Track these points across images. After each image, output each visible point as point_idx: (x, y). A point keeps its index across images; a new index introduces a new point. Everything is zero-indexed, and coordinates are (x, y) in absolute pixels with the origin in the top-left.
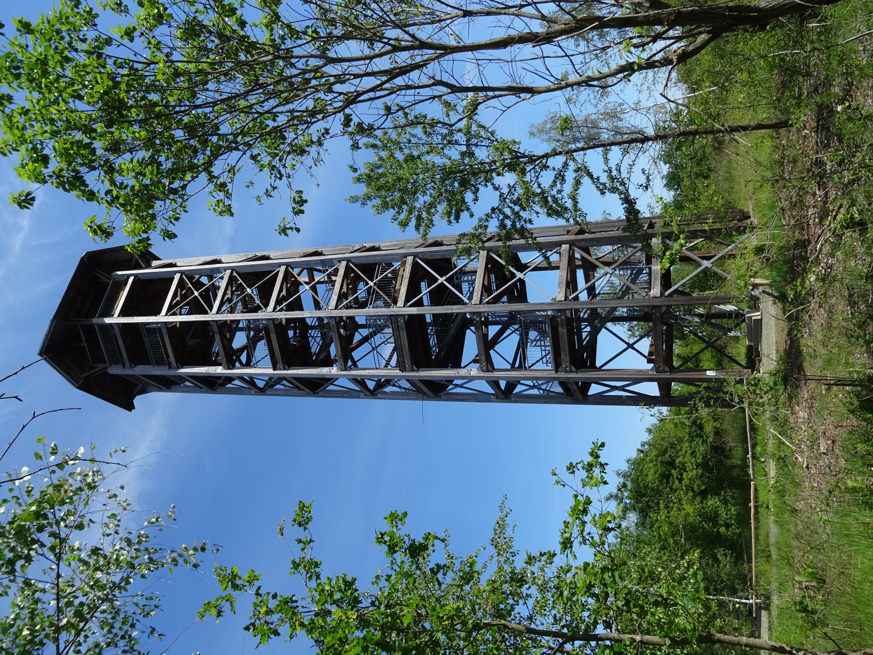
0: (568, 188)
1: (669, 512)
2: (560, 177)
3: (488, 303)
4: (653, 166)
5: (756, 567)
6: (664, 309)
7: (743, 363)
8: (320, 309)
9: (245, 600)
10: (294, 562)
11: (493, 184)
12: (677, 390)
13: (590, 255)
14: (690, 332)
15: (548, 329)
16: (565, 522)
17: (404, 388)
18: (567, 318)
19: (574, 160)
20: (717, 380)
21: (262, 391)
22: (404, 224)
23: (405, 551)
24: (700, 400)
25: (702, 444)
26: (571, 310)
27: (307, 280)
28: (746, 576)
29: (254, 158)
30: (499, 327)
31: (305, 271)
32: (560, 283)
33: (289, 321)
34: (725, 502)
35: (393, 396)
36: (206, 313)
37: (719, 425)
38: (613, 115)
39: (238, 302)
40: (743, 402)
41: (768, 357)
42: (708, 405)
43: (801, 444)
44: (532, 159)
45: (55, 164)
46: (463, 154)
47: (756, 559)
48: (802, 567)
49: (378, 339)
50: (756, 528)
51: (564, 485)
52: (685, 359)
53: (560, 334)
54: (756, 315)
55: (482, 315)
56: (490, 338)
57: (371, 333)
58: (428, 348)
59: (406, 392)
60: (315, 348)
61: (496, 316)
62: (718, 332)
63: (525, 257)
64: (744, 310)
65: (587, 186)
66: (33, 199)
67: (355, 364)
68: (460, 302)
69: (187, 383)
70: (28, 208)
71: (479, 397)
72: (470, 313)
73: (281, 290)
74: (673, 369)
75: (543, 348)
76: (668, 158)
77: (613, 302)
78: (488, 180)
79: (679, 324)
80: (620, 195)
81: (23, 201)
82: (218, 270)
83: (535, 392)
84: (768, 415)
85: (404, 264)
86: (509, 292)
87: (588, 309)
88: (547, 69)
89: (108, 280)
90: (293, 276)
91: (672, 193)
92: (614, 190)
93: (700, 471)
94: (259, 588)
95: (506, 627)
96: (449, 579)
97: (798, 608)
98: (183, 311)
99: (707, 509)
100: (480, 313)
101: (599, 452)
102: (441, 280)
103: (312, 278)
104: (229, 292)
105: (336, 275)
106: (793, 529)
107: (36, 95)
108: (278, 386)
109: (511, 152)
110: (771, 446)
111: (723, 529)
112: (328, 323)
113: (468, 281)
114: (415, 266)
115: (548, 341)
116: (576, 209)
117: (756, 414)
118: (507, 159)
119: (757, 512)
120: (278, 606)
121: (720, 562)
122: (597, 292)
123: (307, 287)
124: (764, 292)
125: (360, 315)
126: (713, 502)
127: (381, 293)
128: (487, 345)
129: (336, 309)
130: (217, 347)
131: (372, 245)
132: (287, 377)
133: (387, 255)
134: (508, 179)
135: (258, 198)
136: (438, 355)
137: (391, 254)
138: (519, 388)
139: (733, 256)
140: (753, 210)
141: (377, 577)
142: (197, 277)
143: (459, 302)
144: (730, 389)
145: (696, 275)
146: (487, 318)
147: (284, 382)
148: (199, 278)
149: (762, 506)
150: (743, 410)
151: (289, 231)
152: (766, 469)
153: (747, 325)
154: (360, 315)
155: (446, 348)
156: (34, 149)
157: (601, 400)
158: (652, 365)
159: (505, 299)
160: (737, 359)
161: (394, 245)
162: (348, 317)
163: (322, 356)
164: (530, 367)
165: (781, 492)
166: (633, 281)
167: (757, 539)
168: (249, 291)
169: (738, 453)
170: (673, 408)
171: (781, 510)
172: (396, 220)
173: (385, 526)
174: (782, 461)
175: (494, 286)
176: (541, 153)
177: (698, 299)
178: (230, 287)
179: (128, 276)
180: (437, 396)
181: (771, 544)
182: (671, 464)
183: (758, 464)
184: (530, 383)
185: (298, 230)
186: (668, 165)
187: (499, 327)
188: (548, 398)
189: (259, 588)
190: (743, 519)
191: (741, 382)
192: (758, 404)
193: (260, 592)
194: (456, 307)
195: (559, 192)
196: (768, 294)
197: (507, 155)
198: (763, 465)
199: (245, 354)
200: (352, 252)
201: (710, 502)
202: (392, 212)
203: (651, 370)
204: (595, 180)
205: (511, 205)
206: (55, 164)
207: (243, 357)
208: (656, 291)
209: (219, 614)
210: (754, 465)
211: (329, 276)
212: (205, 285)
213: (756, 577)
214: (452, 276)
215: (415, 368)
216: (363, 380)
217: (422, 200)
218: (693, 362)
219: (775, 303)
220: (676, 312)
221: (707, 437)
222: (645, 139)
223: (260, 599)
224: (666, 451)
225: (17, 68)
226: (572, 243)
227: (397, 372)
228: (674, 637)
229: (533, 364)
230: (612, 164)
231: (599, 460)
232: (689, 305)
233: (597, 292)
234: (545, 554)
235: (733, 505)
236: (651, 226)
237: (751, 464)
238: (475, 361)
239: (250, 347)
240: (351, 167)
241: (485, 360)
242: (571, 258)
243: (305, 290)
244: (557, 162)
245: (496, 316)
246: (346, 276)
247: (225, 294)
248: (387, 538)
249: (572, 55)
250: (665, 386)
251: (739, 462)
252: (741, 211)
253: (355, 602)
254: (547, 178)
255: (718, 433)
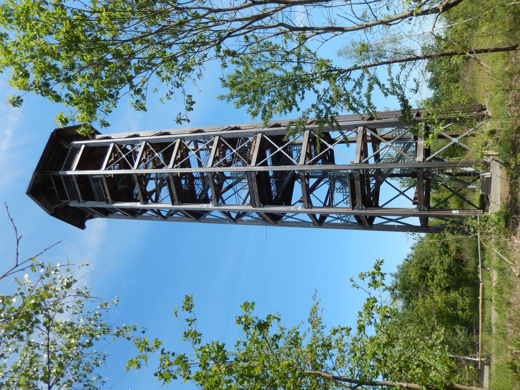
0: (364, 90)
1: (424, 300)
2: (359, 84)
3: (309, 164)
4: (422, 77)
5: (482, 337)
6: (425, 170)
7: (477, 205)
8: (202, 167)
9: (155, 358)
10: (185, 333)
11: (314, 89)
12: (432, 222)
13: (377, 133)
14: (443, 185)
15: (348, 181)
16: (359, 312)
17: (255, 218)
18: (360, 174)
19: (368, 72)
20: (460, 217)
21: (165, 218)
22: (255, 114)
23: (256, 327)
24: (447, 230)
25: (448, 257)
26: (363, 169)
27: (194, 148)
28: (474, 343)
29: (158, 73)
30: (316, 179)
31: (192, 142)
32: (356, 152)
33: (182, 174)
34: (462, 295)
35: (249, 223)
36: (129, 168)
37: (459, 245)
38: (394, 41)
39: (150, 162)
40: (476, 232)
41: (495, 203)
42: (452, 233)
43: (515, 261)
44: (341, 71)
45: (34, 77)
46: (296, 69)
47: (482, 332)
48: (513, 340)
49: (238, 186)
50: (483, 313)
51: (358, 288)
52: (438, 201)
53: (356, 185)
54: (487, 175)
55: (305, 172)
56: (310, 186)
57: (234, 182)
58: (270, 192)
59: (255, 220)
60: (198, 191)
61: (314, 173)
62: (461, 186)
63: (335, 135)
64: (479, 171)
65: (376, 90)
66: (22, 101)
67: (223, 201)
68: (291, 163)
69: (118, 213)
70: (18, 106)
71: (302, 224)
72: (297, 171)
73: (177, 155)
74: (429, 209)
75: (344, 194)
76: (430, 68)
77: (391, 164)
78: (310, 86)
79: (435, 180)
80: (398, 96)
81: (15, 102)
82: (138, 142)
83: (339, 221)
84: (493, 241)
85: (255, 138)
86: (323, 157)
87: (374, 169)
88: (353, 13)
89: (68, 147)
90: (185, 146)
91: (433, 91)
92: (393, 93)
93: (446, 275)
94: (163, 350)
95: (320, 375)
96: (281, 343)
97: (509, 366)
98: (116, 167)
99: (450, 299)
100: (304, 171)
101: (381, 267)
102: (279, 149)
103: (196, 147)
104: (144, 155)
105: (212, 145)
106: (508, 315)
107: (22, 33)
108: (175, 215)
109: (327, 67)
110: (495, 261)
111: (460, 313)
112: (207, 176)
113: (296, 150)
114: (263, 140)
115: (348, 189)
116: (369, 104)
117: (485, 240)
118: (324, 72)
119: (483, 303)
120: (176, 360)
121: (457, 334)
122: (381, 158)
123: (194, 153)
124: (493, 159)
125: (227, 171)
126: (454, 295)
127: (241, 157)
128: (309, 191)
129: (212, 167)
130: (137, 190)
131: (235, 126)
132: (181, 210)
133: (245, 133)
134: (325, 84)
135: (161, 100)
136: (277, 196)
137: (247, 132)
138: (328, 219)
139: (473, 135)
140: (488, 104)
141: (238, 342)
142: (124, 145)
143: (290, 163)
144: (469, 223)
145: (448, 147)
146: (308, 174)
147: (179, 213)
148: (126, 146)
149: (487, 299)
150: (477, 237)
151: (183, 122)
152: (491, 275)
153: (481, 180)
154: (227, 171)
155: (282, 193)
156: (20, 68)
157: (382, 227)
158: (416, 206)
159: (320, 161)
160: (473, 202)
161: (250, 126)
162: (219, 172)
163: (203, 197)
164: (335, 206)
165: (500, 291)
166: (405, 151)
167: (483, 320)
168: (157, 155)
169: (471, 264)
170: (430, 234)
171: (499, 304)
172: (249, 111)
173: (242, 312)
174: (501, 270)
175: (313, 154)
176: (347, 68)
177: (449, 163)
178: (145, 152)
179: (81, 145)
180: (275, 223)
181: (492, 323)
182: (427, 269)
183: (485, 272)
184: (336, 216)
185: (189, 121)
186: (431, 73)
187: (316, 179)
188: (347, 226)
189: (163, 350)
190: (474, 306)
191: (476, 218)
192: (487, 234)
193: (164, 352)
194: (288, 166)
195: (358, 93)
196: (496, 161)
197: (324, 69)
198: (488, 273)
199: (154, 194)
200: (222, 131)
201: (452, 295)
202: (247, 106)
203: (415, 209)
204: (382, 86)
205: (325, 103)
206: (34, 77)
207: (153, 197)
208: (420, 157)
209: (139, 366)
210: (482, 272)
211: (207, 145)
212: (129, 151)
213: (482, 344)
214: (286, 147)
215: (262, 205)
216: (229, 212)
217: (266, 99)
218: (443, 204)
219: (501, 168)
220: (433, 171)
221: (451, 253)
222: (418, 58)
223: (164, 356)
224: (423, 260)
225: (9, 15)
226: (365, 126)
227: (250, 208)
228: (428, 385)
229: (338, 204)
230: (394, 76)
231: (381, 271)
232: (442, 167)
233: (381, 158)
234: (344, 328)
235: (468, 297)
236: (418, 115)
237: (480, 272)
238: (300, 201)
239: (157, 191)
240: (221, 79)
241: (307, 201)
242: (364, 136)
243: (192, 154)
244: (356, 75)
245: (314, 173)
246: (218, 146)
247: (142, 156)
248: (243, 319)
249: (370, 2)
250: (424, 220)
251: (472, 270)
252: (480, 105)
253: (225, 359)
254: (349, 85)
255: (458, 250)
